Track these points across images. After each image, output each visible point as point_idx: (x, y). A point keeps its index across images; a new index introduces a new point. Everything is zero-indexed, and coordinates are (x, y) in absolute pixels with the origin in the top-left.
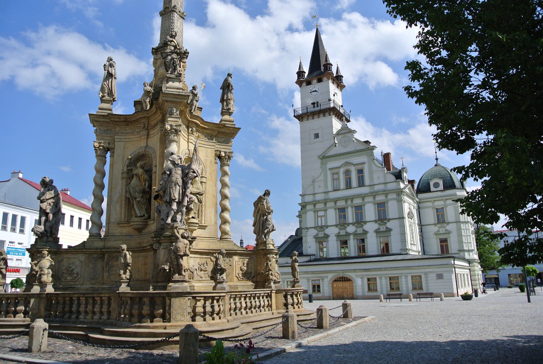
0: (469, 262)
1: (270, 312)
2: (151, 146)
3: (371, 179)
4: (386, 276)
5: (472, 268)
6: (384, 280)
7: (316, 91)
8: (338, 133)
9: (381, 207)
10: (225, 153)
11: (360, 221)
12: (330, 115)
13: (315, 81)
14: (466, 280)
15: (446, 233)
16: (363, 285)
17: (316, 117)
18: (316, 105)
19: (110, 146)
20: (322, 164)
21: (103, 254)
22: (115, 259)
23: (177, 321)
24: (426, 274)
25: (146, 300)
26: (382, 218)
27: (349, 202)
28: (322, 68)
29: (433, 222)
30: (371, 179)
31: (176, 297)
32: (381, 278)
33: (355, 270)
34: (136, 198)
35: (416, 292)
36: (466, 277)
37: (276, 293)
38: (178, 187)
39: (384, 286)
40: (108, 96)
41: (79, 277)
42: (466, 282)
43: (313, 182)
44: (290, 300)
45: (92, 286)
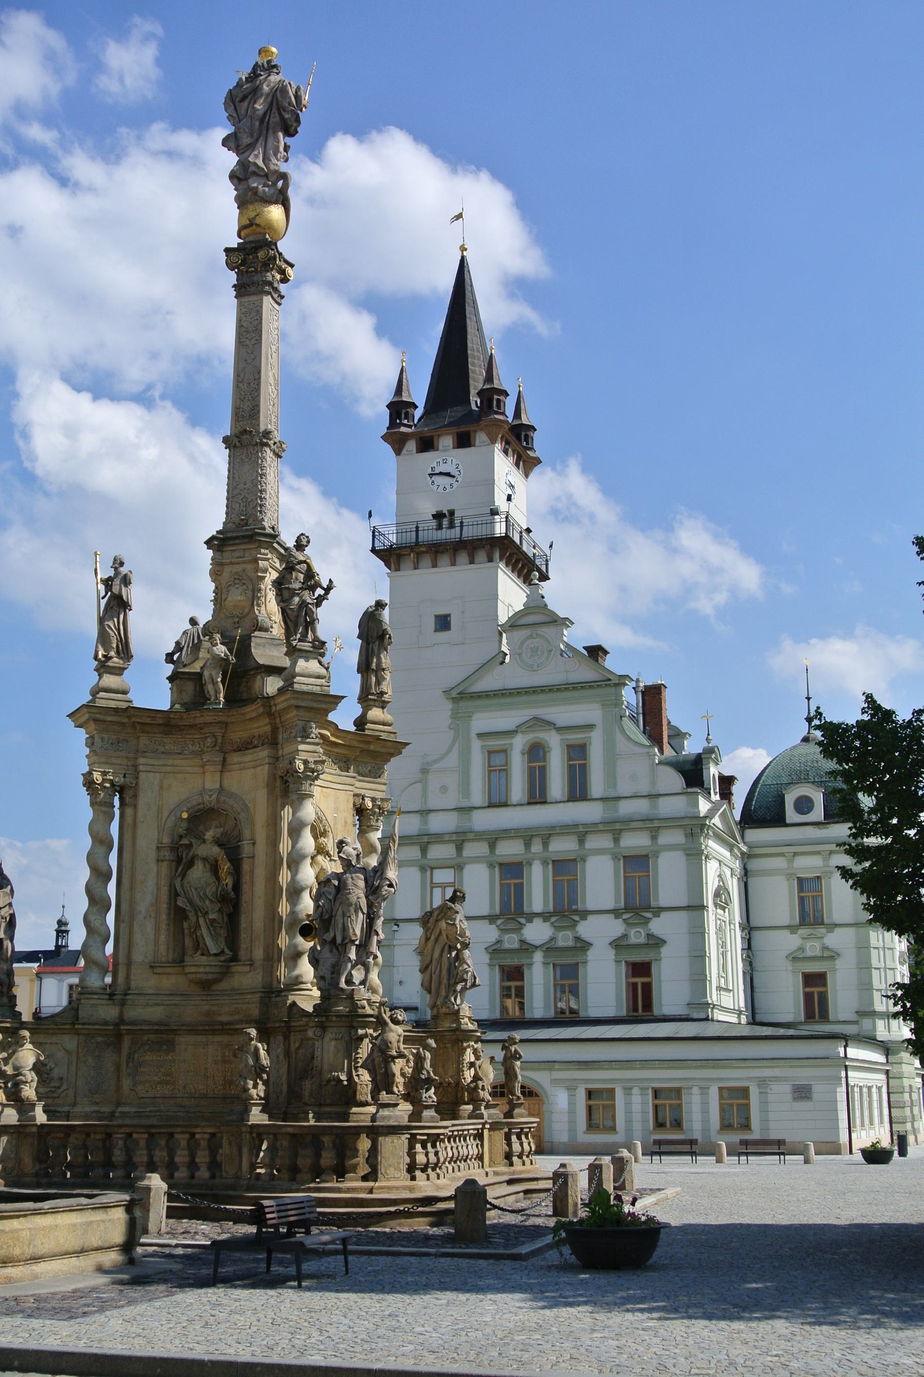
0: (887, 1049)
1: (481, 1170)
2: (234, 790)
3: (611, 777)
4: (646, 1085)
5: (894, 1069)
6: (636, 1098)
7: (448, 474)
8: (514, 624)
9: (637, 865)
10: (374, 800)
11: (566, 911)
12: (491, 560)
13: (446, 441)
14: (875, 1104)
15: (822, 958)
16: (572, 1111)
17: (444, 559)
18: (445, 522)
19: (128, 780)
20: (455, 716)
21: (119, 1036)
22: (147, 1047)
23: (388, 1180)
24: (763, 1083)
25: (326, 1140)
26: (637, 905)
27: (537, 847)
28: (475, 401)
29: (786, 921)
30: (611, 777)
31: (386, 1135)
32: (628, 1091)
33: (549, 1065)
34: (207, 913)
35: (736, 1137)
36: (875, 1096)
37: (490, 1130)
38: (360, 915)
39: (637, 1117)
40: (115, 650)
41: (64, 1087)
42: (876, 1112)
43: (424, 771)
44: (516, 1147)
45: (96, 1108)
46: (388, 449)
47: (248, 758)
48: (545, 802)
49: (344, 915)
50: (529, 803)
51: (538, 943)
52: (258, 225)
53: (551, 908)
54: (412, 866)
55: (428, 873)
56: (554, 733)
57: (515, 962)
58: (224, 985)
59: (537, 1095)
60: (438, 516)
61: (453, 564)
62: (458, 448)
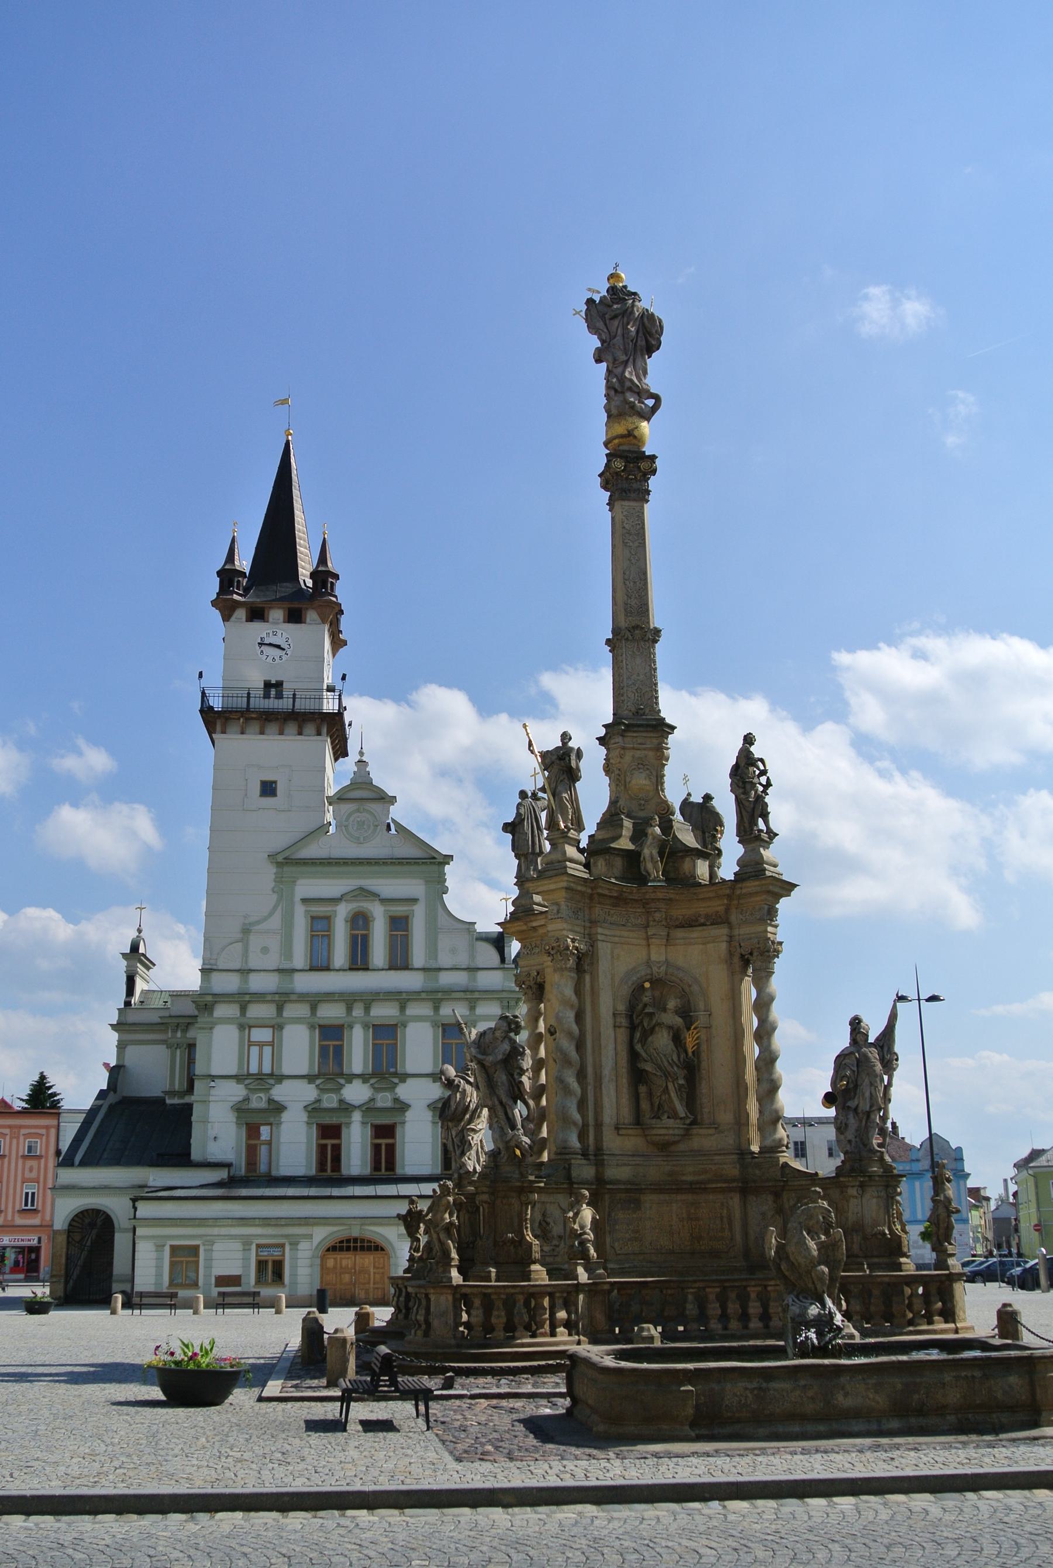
7: (278, 647)
8: (340, 798)
11: (386, 1071)
12: (319, 734)
13: (277, 614)
17: (273, 728)
18: (273, 692)
20: (279, 879)
27: (358, 1011)
43: (246, 931)
46: (216, 614)
47: (695, 935)
48: (367, 969)
49: (871, 1084)
50: (351, 969)
51: (357, 1103)
52: (635, 437)
53: (370, 1070)
54: (230, 1023)
55: (247, 1031)
56: (377, 903)
57: (333, 1120)
58: (682, 1147)
59: (382, 1249)
60: (268, 685)
61: (281, 733)
62: (289, 622)
